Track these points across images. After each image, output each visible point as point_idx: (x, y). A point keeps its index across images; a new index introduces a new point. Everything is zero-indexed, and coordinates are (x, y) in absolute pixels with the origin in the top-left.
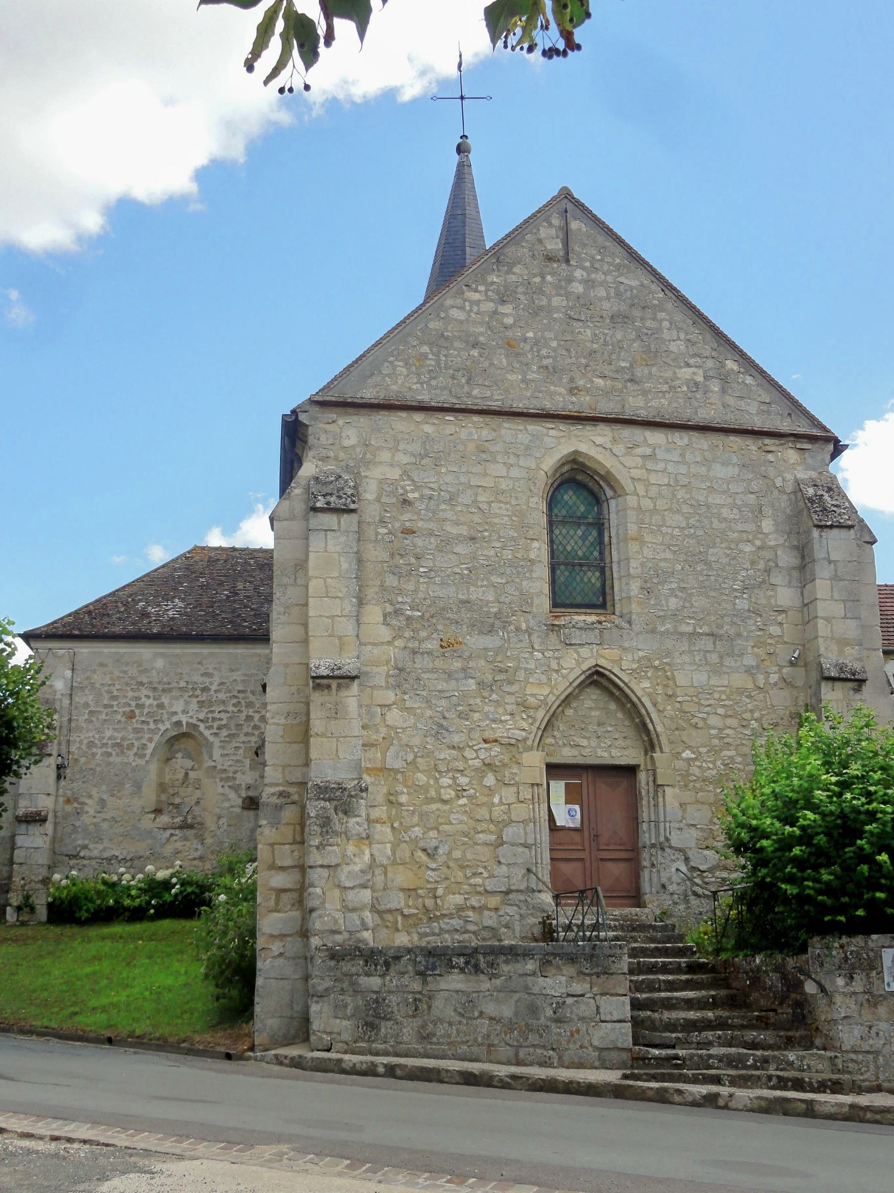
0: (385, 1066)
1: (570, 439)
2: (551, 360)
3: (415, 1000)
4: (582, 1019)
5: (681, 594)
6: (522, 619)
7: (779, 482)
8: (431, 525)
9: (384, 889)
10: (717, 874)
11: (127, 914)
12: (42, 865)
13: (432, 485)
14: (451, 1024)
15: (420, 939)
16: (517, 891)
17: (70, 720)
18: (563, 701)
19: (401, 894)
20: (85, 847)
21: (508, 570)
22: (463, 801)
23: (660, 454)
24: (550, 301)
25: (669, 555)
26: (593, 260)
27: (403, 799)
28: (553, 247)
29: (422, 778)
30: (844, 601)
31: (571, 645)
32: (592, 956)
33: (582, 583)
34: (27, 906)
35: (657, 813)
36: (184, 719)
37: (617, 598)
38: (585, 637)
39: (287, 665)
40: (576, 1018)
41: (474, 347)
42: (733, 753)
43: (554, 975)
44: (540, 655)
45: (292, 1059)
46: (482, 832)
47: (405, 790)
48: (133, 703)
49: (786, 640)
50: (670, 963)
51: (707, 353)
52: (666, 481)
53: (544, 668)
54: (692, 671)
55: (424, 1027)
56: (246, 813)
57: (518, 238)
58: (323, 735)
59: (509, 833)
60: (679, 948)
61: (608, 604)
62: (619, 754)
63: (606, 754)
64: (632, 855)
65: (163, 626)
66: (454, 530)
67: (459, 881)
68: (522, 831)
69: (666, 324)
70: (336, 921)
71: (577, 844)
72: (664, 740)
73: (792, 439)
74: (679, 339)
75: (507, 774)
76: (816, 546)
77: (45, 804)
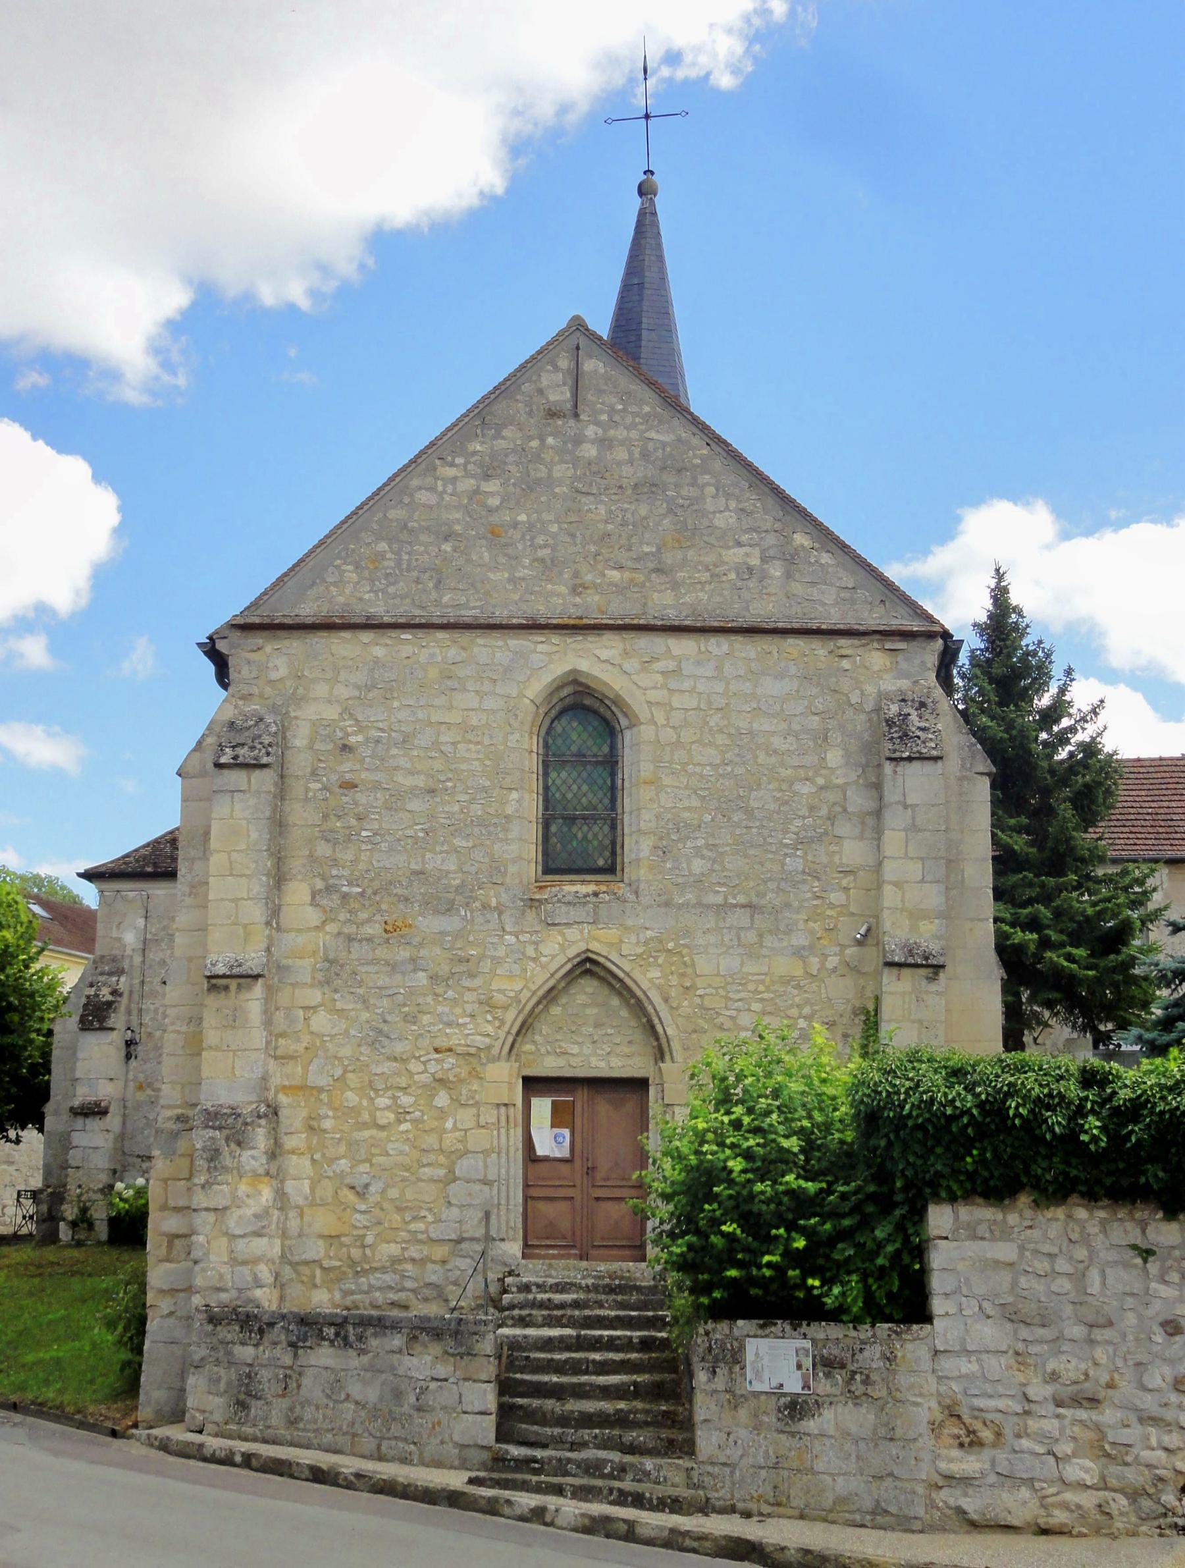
0: (243, 1454)
1: (566, 654)
2: (548, 551)
3: (286, 1376)
4: (444, 1408)
5: (710, 854)
6: (492, 893)
7: (855, 698)
8: (379, 776)
9: (300, 1236)
12: (103, 1170)
13: (381, 725)
14: (317, 1408)
15: (343, 1297)
16: (472, 1239)
17: (143, 982)
18: (544, 997)
19: (321, 1242)
21: (476, 829)
22: (405, 1127)
23: (688, 668)
24: (550, 470)
25: (695, 803)
26: (612, 411)
27: (327, 1124)
28: (558, 398)
29: (352, 1098)
30: (922, 859)
31: (555, 925)
32: (457, 1333)
33: (581, 840)
34: (83, 1221)
38: (574, 914)
39: (190, 959)
40: (439, 1407)
41: (446, 539)
43: (421, 1353)
44: (513, 939)
46: (429, 1165)
47: (330, 1113)
49: (852, 909)
50: (619, 1338)
51: (768, 526)
52: (694, 704)
53: (516, 956)
54: (719, 955)
55: (291, 1409)
57: (512, 389)
58: (217, 1048)
59: (463, 1167)
60: (648, 1318)
62: (620, 1064)
63: (602, 1064)
66: (408, 782)
67: (394, 1226)
68: (481, 1164)
69: (711, 490)
70: (221, 1276)
71: (565, 1178)
72: (676, 1046)
73: (878, 637)
74: (727, 508)
75: (464, 1092)
77: (105, 1091)
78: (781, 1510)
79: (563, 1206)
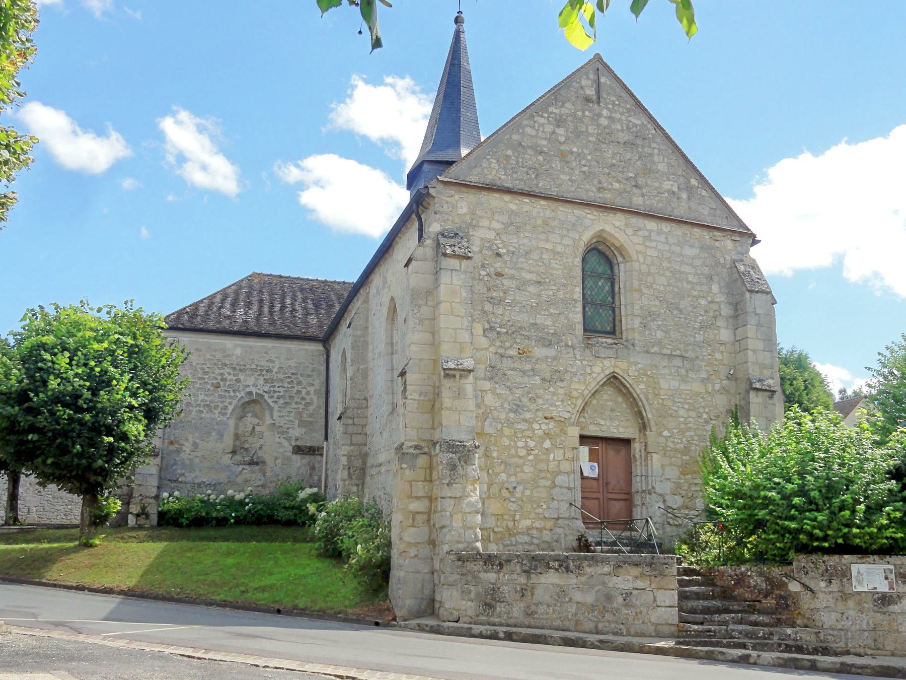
0: (505, 633)
7: (722, 261)
8: (512, 272)
10: (682, 511)
11: (214, 522)
14: (548, 606)
19: (493, 518)
20: (183, 475)
22: (531, 457)
26: (614, 104)
27: (495, 454)
35: (647, 471)
36: (254, 391)
37: (623, 328)
42: (692, 434)
45: (432, 627)
48: (219, 378)
55: (528, 607)
56: (294, 456)
58: (450, 409)
59: (559, 480)
61: (617, 333)
63: (615, 431)
64: (628, 498)
65: (241, 326)
66: (528, 276)
68: (567, 479)
69: (656, 151)
72: (652, 423)
76: (748, 304)
78: (879, 652)
79: (596, 502)
